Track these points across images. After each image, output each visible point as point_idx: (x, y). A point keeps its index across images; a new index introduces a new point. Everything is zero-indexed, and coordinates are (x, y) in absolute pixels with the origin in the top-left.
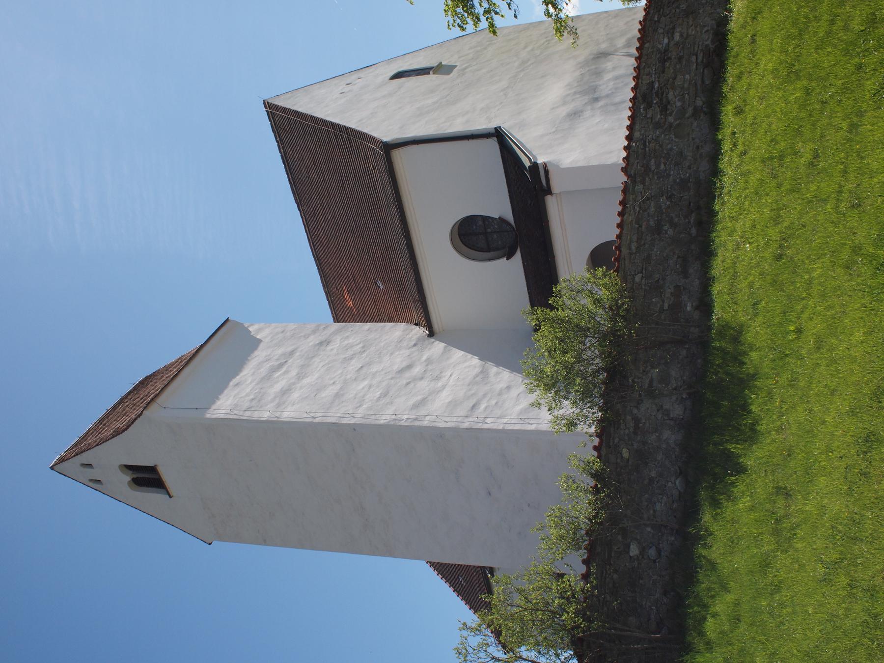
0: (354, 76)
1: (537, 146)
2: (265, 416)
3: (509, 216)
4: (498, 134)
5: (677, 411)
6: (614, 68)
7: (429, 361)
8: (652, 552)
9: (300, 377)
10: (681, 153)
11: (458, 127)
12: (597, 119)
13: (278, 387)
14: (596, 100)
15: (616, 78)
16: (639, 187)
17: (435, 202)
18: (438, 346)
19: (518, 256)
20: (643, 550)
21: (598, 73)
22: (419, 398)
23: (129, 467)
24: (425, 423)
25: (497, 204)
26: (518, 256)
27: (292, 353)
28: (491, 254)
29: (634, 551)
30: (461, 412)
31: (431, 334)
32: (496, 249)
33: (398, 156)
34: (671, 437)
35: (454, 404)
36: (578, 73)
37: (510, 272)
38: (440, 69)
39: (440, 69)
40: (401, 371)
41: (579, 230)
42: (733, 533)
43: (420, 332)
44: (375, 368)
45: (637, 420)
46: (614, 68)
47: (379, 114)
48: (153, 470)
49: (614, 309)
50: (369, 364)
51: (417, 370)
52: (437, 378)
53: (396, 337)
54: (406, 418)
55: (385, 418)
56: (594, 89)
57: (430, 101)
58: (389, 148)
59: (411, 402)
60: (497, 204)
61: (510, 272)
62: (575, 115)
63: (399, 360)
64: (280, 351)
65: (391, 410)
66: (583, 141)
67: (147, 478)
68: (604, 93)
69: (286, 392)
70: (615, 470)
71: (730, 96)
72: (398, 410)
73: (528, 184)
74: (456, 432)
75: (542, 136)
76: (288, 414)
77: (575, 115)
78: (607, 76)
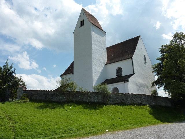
0: (145, 49)
1: (131, 80)
2: (92, 42)
3: (122, 75)
4: (134, 74)
5: (96, 101)
6: (145, 89)
7: (101, 65)
8: (80, 99)
9: (98, 46)
10: (128, 100)
11: (135, 68)
12: (136, 88)
13: (96, 43)
14: (139, 87)
15: (143, 90)
16: (123, 95)
17: (124, 65)
18: (103, 66)
19: (117, 77)
20: (80, 98)
21: (144, 87)
22: (96, 64)
23: (83, 21)
24: (93, 66)
25: (124, 74)
26: (117, 77)
27: (102, 44)
28: (117, 72)
29: (80, 97)
30: (95, 71)
31: (105, 64)
32: (118, 73)
33: (130, 60)
34: (93, 100)
35: (95, 69)
36: (144, 84)
37: (114, 75)
38: (145, 62)
39: (145, 62)
40: (100, 61)
41: (120, 86)
42: (79, 108)
43: (106, 63)
44: (100, 57)
45: (95, 96)
46: (145, 89)
47: (137, 55)
48: (83, 25)
49: (109, 93)
50: (101, 56)
51: (100, 63)
52: (99, 66)
53: (104, 59)
54: (93, 63)
55: (93, 60)
56: (141, 87)
57: (139, 63)
58: (131, 58)
59: (96, 63)
60: (124, 74)
61: (114, 75)
62: (137, 84)
63: (101, 60)
64: (102, 42)
65: (94, 61)
66: (131, 87)
67: (82, 24)
68: (141, 89)
69: (96, 45)
70: (87, 94)
71: (6, 105)
72: (94, 61)
73: (126, 79)
74: (92, 70)
75: (133, 80)
76: (93, 46)
77: (137, 84)
78: (144, 89)
